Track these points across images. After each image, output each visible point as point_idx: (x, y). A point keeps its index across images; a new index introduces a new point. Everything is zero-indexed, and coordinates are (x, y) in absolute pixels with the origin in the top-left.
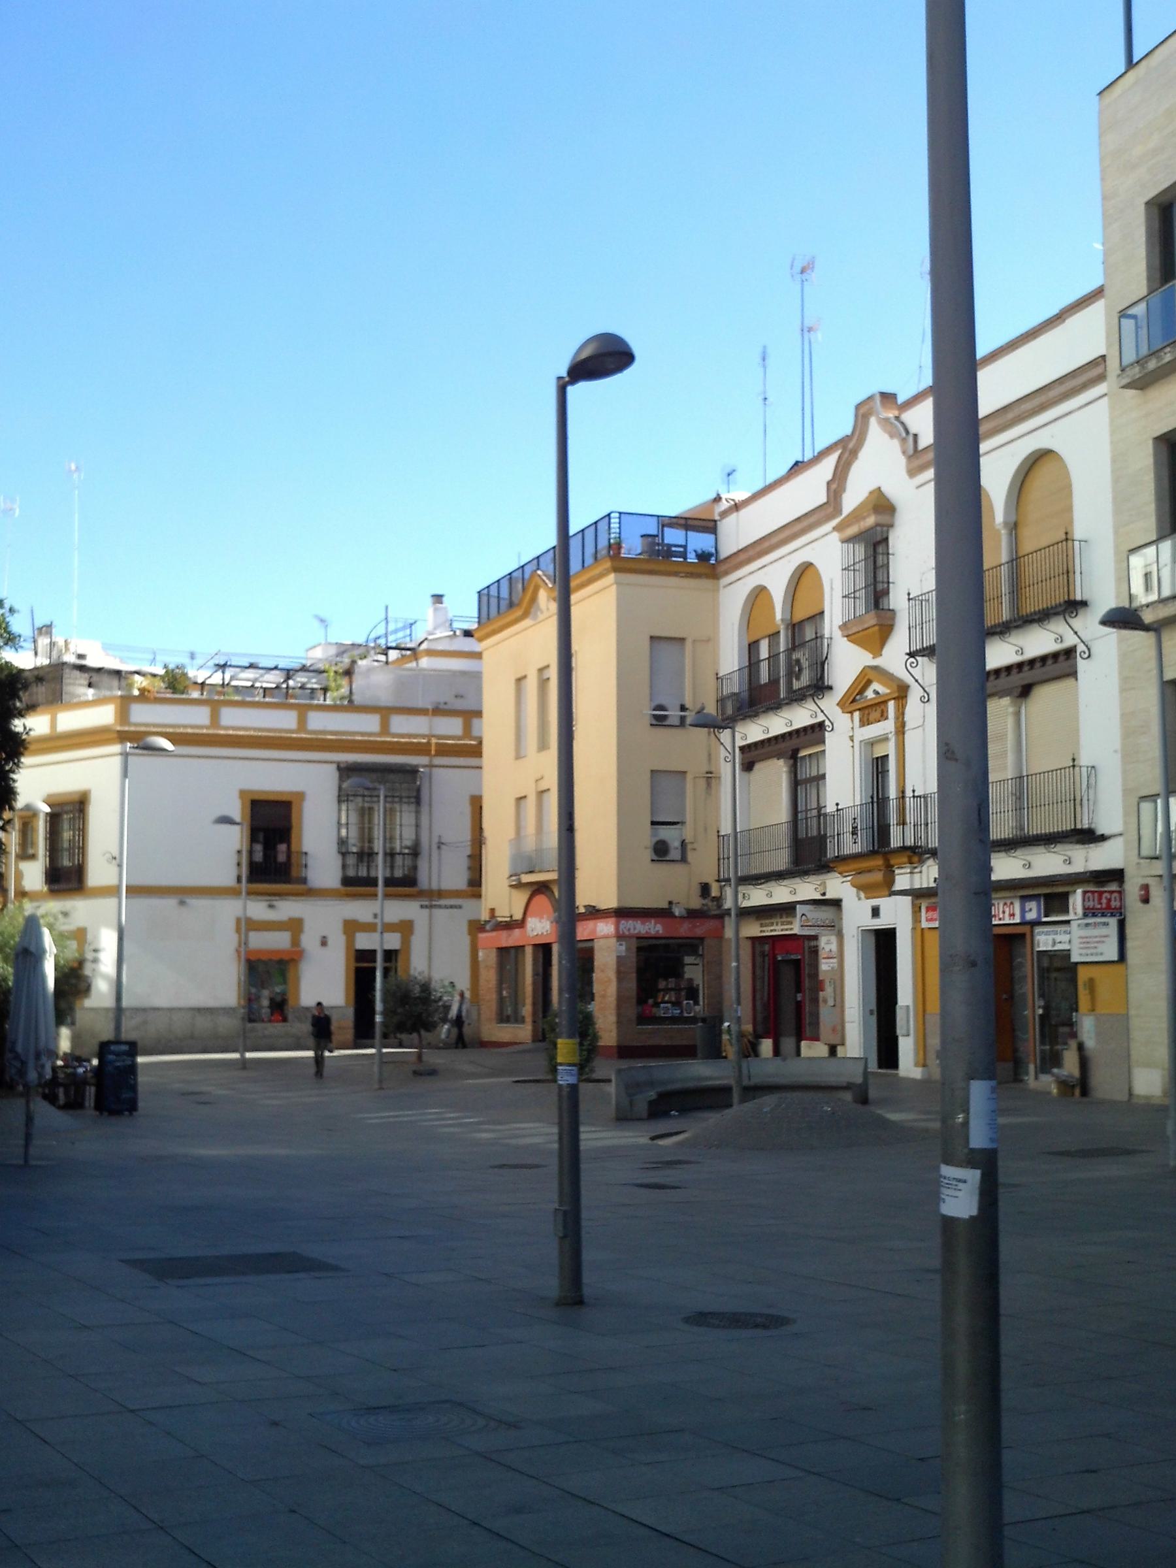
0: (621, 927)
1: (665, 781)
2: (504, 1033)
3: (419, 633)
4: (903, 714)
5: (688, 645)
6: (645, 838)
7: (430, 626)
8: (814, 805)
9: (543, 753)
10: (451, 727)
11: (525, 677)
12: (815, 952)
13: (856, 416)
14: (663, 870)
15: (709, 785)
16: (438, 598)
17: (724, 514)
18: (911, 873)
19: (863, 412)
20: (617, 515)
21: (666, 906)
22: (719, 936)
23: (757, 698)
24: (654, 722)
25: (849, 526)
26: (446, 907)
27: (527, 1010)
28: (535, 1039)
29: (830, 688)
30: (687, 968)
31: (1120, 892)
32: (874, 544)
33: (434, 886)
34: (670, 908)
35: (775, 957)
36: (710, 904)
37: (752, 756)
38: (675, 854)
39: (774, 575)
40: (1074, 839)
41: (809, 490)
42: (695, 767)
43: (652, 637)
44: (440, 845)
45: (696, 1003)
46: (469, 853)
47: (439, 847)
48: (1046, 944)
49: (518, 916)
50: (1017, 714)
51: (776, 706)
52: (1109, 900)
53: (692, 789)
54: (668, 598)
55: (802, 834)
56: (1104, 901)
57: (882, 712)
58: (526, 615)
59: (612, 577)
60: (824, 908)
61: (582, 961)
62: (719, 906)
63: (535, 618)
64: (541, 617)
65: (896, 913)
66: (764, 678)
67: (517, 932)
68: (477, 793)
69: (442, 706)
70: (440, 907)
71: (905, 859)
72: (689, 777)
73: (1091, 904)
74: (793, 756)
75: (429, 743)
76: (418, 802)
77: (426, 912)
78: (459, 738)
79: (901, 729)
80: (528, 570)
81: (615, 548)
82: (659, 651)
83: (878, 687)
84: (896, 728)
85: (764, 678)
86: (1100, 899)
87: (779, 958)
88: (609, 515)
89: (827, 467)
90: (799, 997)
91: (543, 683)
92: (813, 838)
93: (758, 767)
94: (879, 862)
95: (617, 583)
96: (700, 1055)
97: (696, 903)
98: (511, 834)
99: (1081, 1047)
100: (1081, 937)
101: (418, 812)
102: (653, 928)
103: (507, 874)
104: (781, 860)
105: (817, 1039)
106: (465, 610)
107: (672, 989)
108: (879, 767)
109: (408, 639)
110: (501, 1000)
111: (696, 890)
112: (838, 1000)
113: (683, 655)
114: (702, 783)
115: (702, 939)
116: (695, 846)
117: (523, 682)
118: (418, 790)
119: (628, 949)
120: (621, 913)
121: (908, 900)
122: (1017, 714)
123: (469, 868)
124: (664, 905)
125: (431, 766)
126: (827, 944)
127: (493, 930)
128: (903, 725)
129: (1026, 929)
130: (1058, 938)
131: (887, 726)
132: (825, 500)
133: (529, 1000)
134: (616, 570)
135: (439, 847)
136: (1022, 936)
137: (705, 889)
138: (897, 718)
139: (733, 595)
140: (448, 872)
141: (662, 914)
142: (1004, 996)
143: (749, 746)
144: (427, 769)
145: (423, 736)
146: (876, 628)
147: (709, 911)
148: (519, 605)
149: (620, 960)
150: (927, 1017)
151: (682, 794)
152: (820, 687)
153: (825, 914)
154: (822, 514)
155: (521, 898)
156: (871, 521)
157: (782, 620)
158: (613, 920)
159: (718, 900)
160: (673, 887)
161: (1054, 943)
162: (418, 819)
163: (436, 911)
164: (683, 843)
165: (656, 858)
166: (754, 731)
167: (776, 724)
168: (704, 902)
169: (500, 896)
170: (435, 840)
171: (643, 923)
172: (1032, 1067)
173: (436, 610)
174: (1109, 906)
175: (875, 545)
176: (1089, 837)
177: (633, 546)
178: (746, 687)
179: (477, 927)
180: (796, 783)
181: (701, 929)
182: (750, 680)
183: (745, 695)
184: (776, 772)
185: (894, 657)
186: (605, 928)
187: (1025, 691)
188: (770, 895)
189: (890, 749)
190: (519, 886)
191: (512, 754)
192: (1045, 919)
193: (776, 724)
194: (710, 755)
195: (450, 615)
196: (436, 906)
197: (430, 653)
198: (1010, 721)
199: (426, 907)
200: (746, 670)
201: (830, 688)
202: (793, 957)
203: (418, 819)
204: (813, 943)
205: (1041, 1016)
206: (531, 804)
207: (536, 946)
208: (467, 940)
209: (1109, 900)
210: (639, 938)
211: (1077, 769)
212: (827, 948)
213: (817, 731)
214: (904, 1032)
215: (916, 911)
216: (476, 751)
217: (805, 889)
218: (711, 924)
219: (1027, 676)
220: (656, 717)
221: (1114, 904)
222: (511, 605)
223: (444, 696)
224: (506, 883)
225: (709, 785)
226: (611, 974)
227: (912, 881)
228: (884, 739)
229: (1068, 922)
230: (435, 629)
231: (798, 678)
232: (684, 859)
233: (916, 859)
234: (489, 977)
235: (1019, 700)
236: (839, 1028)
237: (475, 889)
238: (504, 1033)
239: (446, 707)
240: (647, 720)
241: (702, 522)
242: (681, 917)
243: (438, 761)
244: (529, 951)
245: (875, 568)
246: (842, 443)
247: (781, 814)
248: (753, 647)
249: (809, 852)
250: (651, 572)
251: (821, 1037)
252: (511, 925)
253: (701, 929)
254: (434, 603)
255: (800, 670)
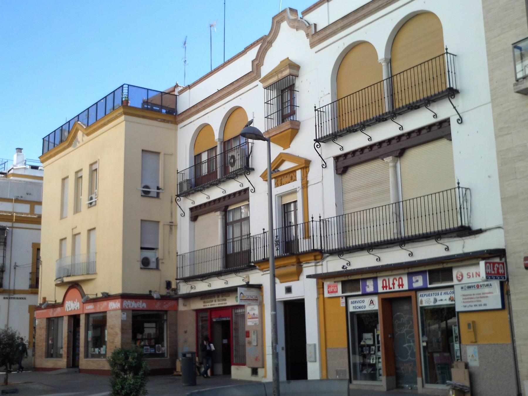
0: (124, 304)
1: (148, 226)
2: (50, 363)
3: (9, 166)
4: (307, 177)
5: (161, 156)
6: (138, 255)
7: (15, 162)
8: (231, 237)
9: (77, 215)
10: (24, 209)
11: (67, 177)
12: (243, 316)
13: (273, 23)
14: (146, 273)
15: (171, 229)
16: (19, 150)
17: (181, 92)
18: (316, 266)
19: (277, 21)
20: (127, 86)
21: (148, 293)
22: (176, 310)
23: (199, 182)
24: (143, 194)
25: (270, 78)
26: (17, 298)
27: (64, 351)
28: (68, 366)
29: (253, 169)
30: (145, 329)
31: (503, 264)
32: (285, 88)
33: (12, 288)
34: (150, 294)
35: (211, 319)
36: (171, 292)
37: (196, 213)
38: (153, 265)
39: (214, 117)
40: (455, 234)
41: (243, 66)
42: (164, 220)
43: (143, 150)
44: (16, 267)
45: (163, 346)
46: (30, 271)
47: (15, 268)
48: (428, 302)
49: (60, 300)
50: (395, 167)
51: (217, 183)
52: (498, 269)
53: (162, 230)
54: (152, 131)
55: (230, 251)
56: (496, 269)
57: (292, 177)
58: (69, 145)
59: (123, 118)
60: (253, 289)
61: (99, 323)
62: (176, 293)
63: (74, 147)
64: (78, 145)
65: (304, 289)
66: (205, 170)
67: (59, 309)
68: (35, 241)
69: (19, 198)
70: (14, 298)
71: (313, 258)
72: (161, 225)
73: (489, 270)
74: (225, 211)
75: (12, 216)
76: (5, 244)
77: (7, 300)
78: (27, 214)
79: (305, 185)
80: (72, 123)
81: (125, 104)
82: (146, 160)
83: (287, 166)
84: (302, 185)
85: (205, 170)
86: (494, 267)
87: (214, 320)
88: (122, 86)
89: (253, 54)
90: (225, 341)
91: (79, 179)
92: (238, 253)
93: (200, 218)
94: (294, 260)
95: (125, 120)
96: (439, 381)
97: (164, 292)
98: (57, 257)
99: (467, 366)
100: (463, 295)
101: (4, 250)
102: (141, 305)
103: (55, 278)
104: (218, 266)
105: (244, 364)
106: (34, 152)
107: (145, 339)
108: (285, 209)
109: (3, 169)
110: (48, 345)
111: (164, 285)
112: (260, 341)
113: (159, 159)
114: (168, 228)
115: (166, 312)
116: (164, 261)
117: (66, 180)
118: (6, 239)
119: (127, 316)
120: (124, 297)
121: (314, 281)
122: (395, 167)
123: (30, 279)
124: (147, 292)
125: (12, 227)
126: (252, 310)
127: (45, 309)
128: (307, 182)
129: (412, 294)
130: (438, 298)
131: (297, 184)
132: (251, 70)
133: (65, 346)
134: (125, 113)
135: (15, 268)
136: (409, 298)
137: (169, 284)
138: (302, 179)
139: (186, 132)
140: (20, 280)
141: (147, 297)
142: (389, 336)
143: (196, 207)
144: (11, 229)
145: (10, 212)
146: (290, 130)
147: (171, 296)
148: (67, 140)
149: (123, 323)
150: (328, 350)
151: (157, 234)
152: (247, 169)
153: (253, 293)
154: (248, 78)
155: (61, 292)
156: (287, 72)
157: (219, 139)
158: (120, 300)
159: (175, 290)
160: (151, 283)
161: (435, 301)
162: (4, 253)
163: (11, 300)
164: (157, 259)
165: (142, 267)
166: (200, 199)
167: (216, 193)
168: (168, 291)
169: (49, 289)
170: (13, 264)
171: (136, 302)
172: (419, 380)
173: (18, 155)
174: (498, 273)
175: (282, 93)
176: (465, 232)
177: (136, 102)
178: (193, 176)
179: (33, 309)
180: (226, 225)
181: (166, 305)
182: (195, 175)
183: (193, 180)
184: (215, 219)
185: (303, 145)
186: (114, 305)
187: (401, 154)
188: (210, 285)
189: (299, 197)
190: (62, 284)
191: (59, 217)
192: (429, 286)
193: (216, 193)
194: (172, 214)
195: (25, 159)
196: (12, 298)
197: (14, 175)
198: (391, 171)
199: (7, 298)
200: (193, 168)
201: (253, 169)
202: (225, 319)
203: (4, 253)
204: (239, 311)
205: (424, 347)
206: (68, 243)
207: (70, 317)
208: (28, 315)
209: (498, 269)
210: (133, 310)
211: (461, 189)
212: (251, 313)
213: (243, 195)
214: (313, 359)
215: (320, 288)
216: (38, 220)
217: (235, 280)
218: (172, 303)
219: (404, 143)
220: (144, 192)
221: (501, 271)
222: (61, 141)
223: (22, 194)
224: (54, 283)
225: (171, 229)
226: (118, 330)
227: (316, 270)
228: (294, 192)
229: (452, 287)
230: (17, 164)
231: (233, 165)
232: (157, 268)
233: (319, 257)
234: (41, 334)
235: (397, 158)
236: (260, 358)
237: (34, 289)
238: (50, 363)
239: (22, 199)
240: (140, 193)
241: (171, 95)
242: (157, 299)
243: (16, 225)
244: (66, 319)
245: (282, 103)
246: (263, 39)
247: (219, 240)
248: (197, 157)
249: (236, 260)
250: (143, 117)
251: (247, 363)
252: (55, 306)
253: (166, 305)
254: (17, 152)
255: (234, 161)
